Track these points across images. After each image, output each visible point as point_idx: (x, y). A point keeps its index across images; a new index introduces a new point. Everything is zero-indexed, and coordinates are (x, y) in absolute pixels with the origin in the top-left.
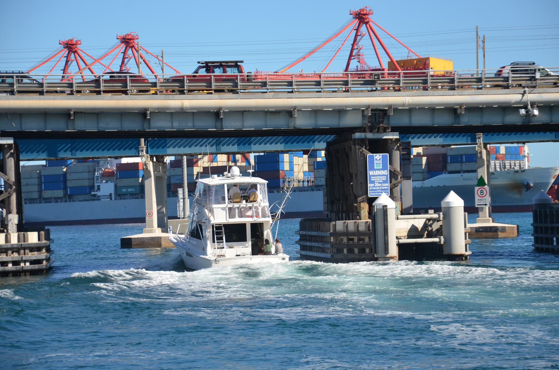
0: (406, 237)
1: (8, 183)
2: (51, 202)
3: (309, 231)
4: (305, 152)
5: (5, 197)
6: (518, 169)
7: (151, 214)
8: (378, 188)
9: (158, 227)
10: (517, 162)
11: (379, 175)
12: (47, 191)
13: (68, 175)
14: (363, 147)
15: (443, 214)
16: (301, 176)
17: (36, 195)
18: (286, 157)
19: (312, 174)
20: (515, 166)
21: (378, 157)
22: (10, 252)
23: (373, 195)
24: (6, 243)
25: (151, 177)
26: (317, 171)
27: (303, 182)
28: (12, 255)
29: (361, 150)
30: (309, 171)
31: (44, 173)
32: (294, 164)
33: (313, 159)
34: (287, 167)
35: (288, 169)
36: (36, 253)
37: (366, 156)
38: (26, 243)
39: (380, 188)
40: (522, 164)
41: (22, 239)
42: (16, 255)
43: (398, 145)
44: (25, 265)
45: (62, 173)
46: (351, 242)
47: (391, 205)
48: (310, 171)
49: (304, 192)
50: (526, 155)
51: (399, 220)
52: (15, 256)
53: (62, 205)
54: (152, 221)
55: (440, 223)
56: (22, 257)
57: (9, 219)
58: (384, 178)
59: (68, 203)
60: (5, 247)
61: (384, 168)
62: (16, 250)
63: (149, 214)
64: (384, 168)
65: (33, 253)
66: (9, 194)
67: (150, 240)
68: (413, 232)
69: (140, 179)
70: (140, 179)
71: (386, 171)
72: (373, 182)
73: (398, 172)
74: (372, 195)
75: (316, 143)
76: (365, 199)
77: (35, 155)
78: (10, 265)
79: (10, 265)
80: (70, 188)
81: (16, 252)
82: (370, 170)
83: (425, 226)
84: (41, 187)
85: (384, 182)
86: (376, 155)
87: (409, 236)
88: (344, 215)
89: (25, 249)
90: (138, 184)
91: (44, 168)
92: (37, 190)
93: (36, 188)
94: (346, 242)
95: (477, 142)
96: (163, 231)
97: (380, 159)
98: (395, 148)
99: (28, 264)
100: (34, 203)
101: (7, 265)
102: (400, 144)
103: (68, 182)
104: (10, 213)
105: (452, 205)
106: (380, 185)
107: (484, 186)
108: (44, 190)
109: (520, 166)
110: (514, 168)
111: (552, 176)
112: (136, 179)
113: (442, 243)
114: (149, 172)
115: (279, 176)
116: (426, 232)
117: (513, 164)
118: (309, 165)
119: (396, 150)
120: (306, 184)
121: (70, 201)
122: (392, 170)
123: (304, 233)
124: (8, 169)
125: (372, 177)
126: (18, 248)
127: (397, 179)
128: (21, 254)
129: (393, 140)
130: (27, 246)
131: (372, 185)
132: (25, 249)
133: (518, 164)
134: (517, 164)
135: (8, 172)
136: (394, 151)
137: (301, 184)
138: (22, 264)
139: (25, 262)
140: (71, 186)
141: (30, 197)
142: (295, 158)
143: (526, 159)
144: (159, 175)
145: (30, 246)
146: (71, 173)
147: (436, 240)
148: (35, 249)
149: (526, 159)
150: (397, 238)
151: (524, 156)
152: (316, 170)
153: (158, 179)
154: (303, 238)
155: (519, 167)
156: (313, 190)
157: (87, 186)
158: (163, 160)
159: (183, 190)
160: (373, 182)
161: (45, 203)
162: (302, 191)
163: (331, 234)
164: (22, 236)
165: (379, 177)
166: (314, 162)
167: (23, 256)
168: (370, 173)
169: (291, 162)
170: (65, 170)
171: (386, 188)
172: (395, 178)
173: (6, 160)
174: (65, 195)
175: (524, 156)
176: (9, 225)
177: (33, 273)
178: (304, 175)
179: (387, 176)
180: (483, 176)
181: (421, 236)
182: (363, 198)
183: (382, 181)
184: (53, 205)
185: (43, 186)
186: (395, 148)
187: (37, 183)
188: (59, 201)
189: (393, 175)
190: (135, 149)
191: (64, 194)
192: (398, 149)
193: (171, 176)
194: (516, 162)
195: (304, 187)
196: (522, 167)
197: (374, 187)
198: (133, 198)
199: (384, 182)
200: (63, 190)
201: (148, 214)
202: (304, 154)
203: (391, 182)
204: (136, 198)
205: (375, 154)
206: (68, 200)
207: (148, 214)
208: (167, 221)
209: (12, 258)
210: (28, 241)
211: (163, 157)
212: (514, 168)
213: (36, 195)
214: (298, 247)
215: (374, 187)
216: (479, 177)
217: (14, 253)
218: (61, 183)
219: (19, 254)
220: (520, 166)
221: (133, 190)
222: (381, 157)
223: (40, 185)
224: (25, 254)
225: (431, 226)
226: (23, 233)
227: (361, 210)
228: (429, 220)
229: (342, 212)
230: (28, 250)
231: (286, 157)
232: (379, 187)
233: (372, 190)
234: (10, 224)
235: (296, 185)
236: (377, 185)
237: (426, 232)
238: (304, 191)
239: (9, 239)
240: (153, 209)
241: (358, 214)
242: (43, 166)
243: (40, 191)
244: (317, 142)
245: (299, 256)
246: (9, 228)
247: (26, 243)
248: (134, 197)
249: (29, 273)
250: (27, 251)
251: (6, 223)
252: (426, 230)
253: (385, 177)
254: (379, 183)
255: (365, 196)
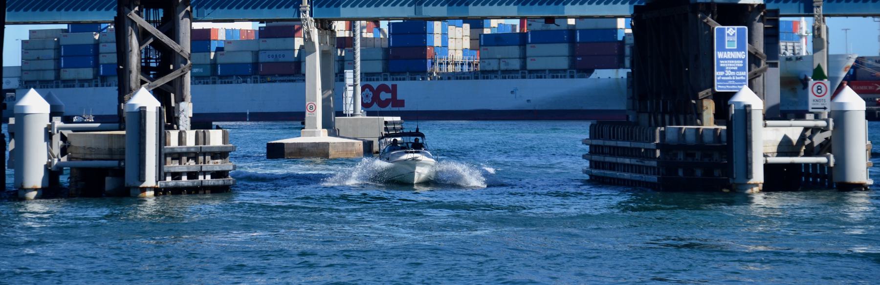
0: (776, 154)
1: (182, 56)
2: (74, 86)
3: (610, 139)
4: (465, 20)
5: (176, 77)
6: (792, 55)
7: (313, 108)
8: (730, 78)
9: (323, 128)
10: (790, 45)
11: (733, 59)
12: (67, 70)
13: (101, 45)
14: (708, 15)
15: (834, 121)
16: (459, 56)
17: (51, 76)
18: (437, 26)
19: (476, 53)
20: (786, 50)
21: (731, 31)
22: (184, 158)
23: (723, 89)
24: (179, 145)
25: (315, 51)
26: (484, 49)
27: (462, 64)
28: (187, 163)
29: (705, 21)
30: (472, 49)
31: (64, 41)
32: (450, 36)
33: (478, 31)
34: (437, 41)
35: (440, 45)
36: (219, 161)
37: (713, 28)
38: (206, 146)
39: (734, 78)
40: (796, 48)
41: (201, 139)
42: (192, 163)
43: (762, 13)
44: (205, 178)
45: (92, 42)
46: (690, 160)
47: (757, 105)
48: (472, 48)
49: (462, 81)
50: (804, 34)
51: (767, 128)
52: (191, 165)
53: (91, 90)
54: (315, 119)
55: (828, 134)
56: (201, 167)
57: (181, 110)
58: (740, 64)
59: (99, 89)
60: (179, 151)
61: (740, 48)
62: (193, 155)
63: (311, 107)
64: (740, 48)
65: (216, 161)
66: (182, 71)
67: (313, 147)
68: (786, 147)
69: (212, 54)
70: (212, 54)
71: (743, 52)
72: (723, 69)
73: (760, 55)
74: (720, 89)
75: (471, 6)
76: (710, 94)
77: (47, 15)
78: (184, 178)
79: (184, 178)
80: (104, 65)
81: (193, 158)
82: (719, 50)
83: (802, 138)
84: (59, 63)
85: (740, 69)
86: (728, 29)
87: (780, 153)
88: (667, 117)
89: (204, 154)
90: (208, 62)
91: (65, 34)
92: (52, 67)
93: (51, 65)
94: (682, 157)
95: (815, 13)
96: (330, 135)
97: (734, 35)
98: (758, 18)
99: (208, 177)
100: (47, 88)
101: (180, 179)
102: (764, 13)
103: (101, 56)
104: (183, 100)
105: (847, 108)
106: (733, 73)
107: (822, 80)
108: (64, 68)
109: (794, 50)
110: (784, 53)
111: (843, 68)
112: (206, 53)
113: (832, 164)
114: (313, 43)
115: (426, 54)
116: (804, 148)
117: (784, 47)
118: (471, 39)
119: (758, 22)
120: (466, 68)
121: (103, 86)
122: (752, 52)
123: (595, 142)
124: (181, 35)
125: (721, 62)
126: (195, 153)
127: (758, 65)
128: (200, 162)
129: (755, 6)
130: (208, 150)
131: (722, 73)
132: (204, 154)
133: (791, 48)
134: (789, 48)
135: (181, 40)
136: (755, 22)
137: (458, 69)
138: (201, 178)
139: (205, 173)
140: (106, 62)
141: (41, 78)
142: (450, 27)
143: (804, 40)
144: (326, 48)
145: (213, 150)
146: (107, 42)
147: (822, 160)
148: (219, 155)
149: (804, 40)
150: (765, 156)
151: (801, 36)
152: (482, 48)
153: (324, 55)
154: (595, 150)
155: (791, 51)
156: (477, 78)
157: (248, 64)
158: (331, 27)
159: (354, 72)
160: (723, 69)
161: (64, 87)
162: (460, 78)
163: (658, 146)
164: (201, 135)
165: (733, 62)
166: (480, 35)
167: (202, 164)
168: (719, 55)
169: (444, 35)
170: (97, 37)
171: (742, 78)
172: (755, 64)
173: (178, 21)
174: (96, 75)
175: (801, 36)
176: (181, 118)
177: (215, 190)
178: (464, 55)
179: (744, 60)
180: (821, 65)
181: (796, 154)
182: (707, 93)
183: (736, 68)
184: (77, 91)
185: (62, 61)
186: (758, 18)
187: (53, 56)
188: (86, 84)
189: (753, 59)
190: (294, 7)
191: (94, 75)
192: (762, 20)
193: (259, 51)
194: (789, 44)
195: (464, 73)
196: (797, 52)
197: (724, 76)
198: (200, 82)
199: (740, 69)
200: (93, 68)
201: (309, 107)
202: (464, 22)
203: (749, 70)
204: (204, 84)
205: (726, 27)
206: (99, 83)
207: (309, 107)
208: (334, 119)
209: (188, 167)
210: (209, 143)
211: (330, 22)
212: (784, 53)
213: (51, 76)
214: (587, 164)
215: (724, 76)
216: (815, 66)
217: (190, 161)
218: (91, 58)
219: (197, 162)
220: (794, 50)
221: (201, 70)
222: (735, 31)
223: (57, 60)
224: (204, 163)
225: (810, 138)
226: (202, 130)
227: (702, 110)
228: (806, 129)
229: (665, 112)
230: (210, 157)
231: (437, 26)
232: (732, 76)
233: (721, 81)
234: (182, 117)
235: (451, 68)
236: (728, 73)
237: (804, 148)
238: (464, 78)
239: (183, 139)
240: (317, 101)
241: (699, 116)
242: (63, 31)
243: (58, 70)
244: (472, 4)
245: (587, 177)
246: (181, 123)
247: (206, 146)
248: (202, 81)
249: (210, 191)
250: (208, 158)
251: (176, 115)
252: (804, 145)
253: (742, 62)
254: (732, 70)
255: (710, 90)
